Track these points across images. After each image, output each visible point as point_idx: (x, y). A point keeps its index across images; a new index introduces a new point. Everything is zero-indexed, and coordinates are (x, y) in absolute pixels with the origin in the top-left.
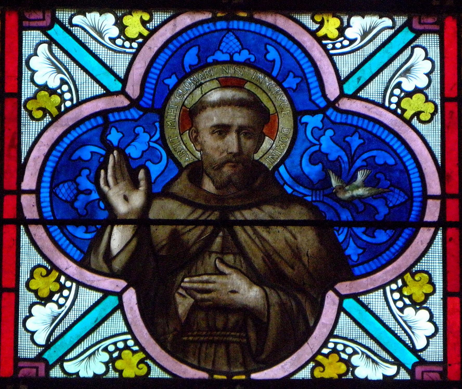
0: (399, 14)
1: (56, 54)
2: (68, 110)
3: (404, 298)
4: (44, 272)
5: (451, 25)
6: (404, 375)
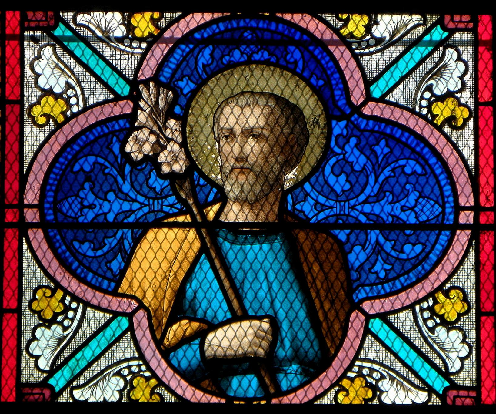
0: (66, 403)
2: (75, 115)
4: (48, 293)
5: (486, 20)
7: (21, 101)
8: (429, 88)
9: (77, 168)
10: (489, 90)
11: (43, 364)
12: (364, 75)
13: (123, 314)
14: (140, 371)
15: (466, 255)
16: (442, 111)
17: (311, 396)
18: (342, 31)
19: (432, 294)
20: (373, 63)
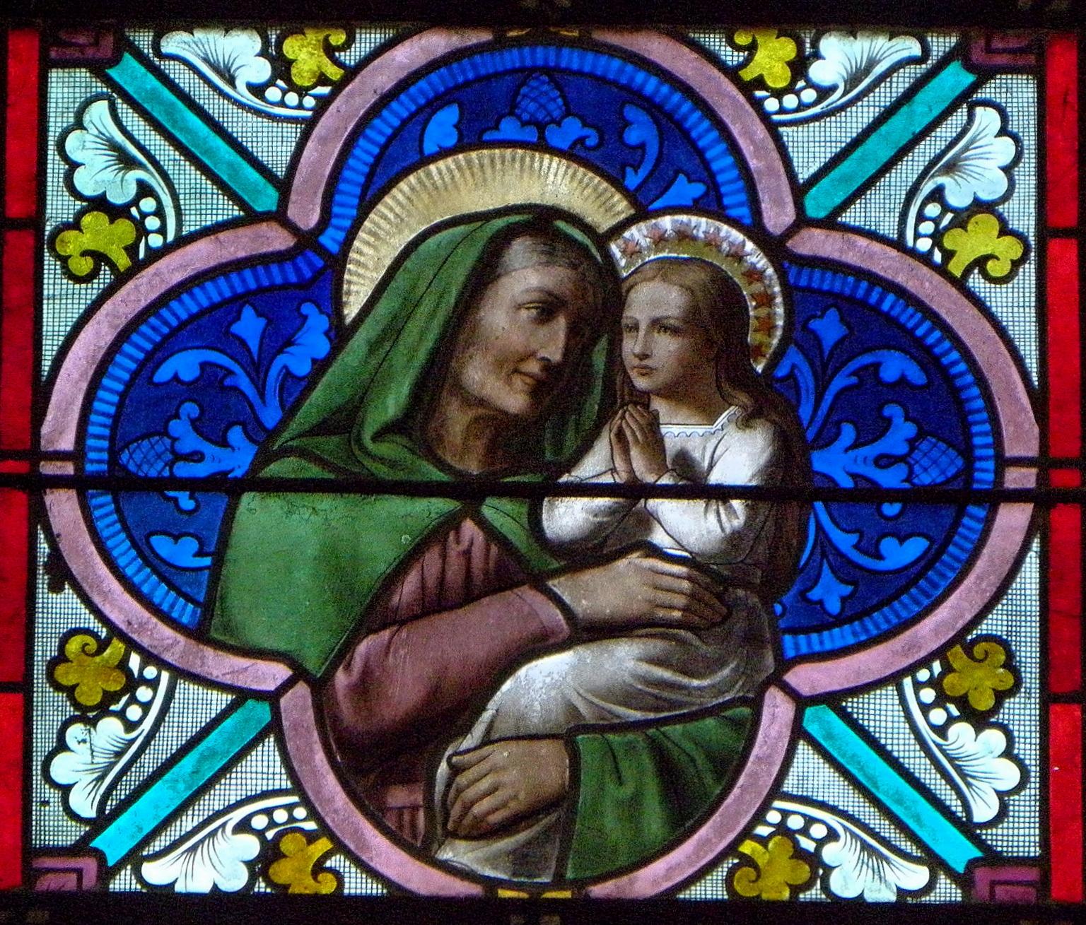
1: (129, 128)
4: (93, 645)
6: (947, 891)
11: (987, 119)
14: (292, 819)
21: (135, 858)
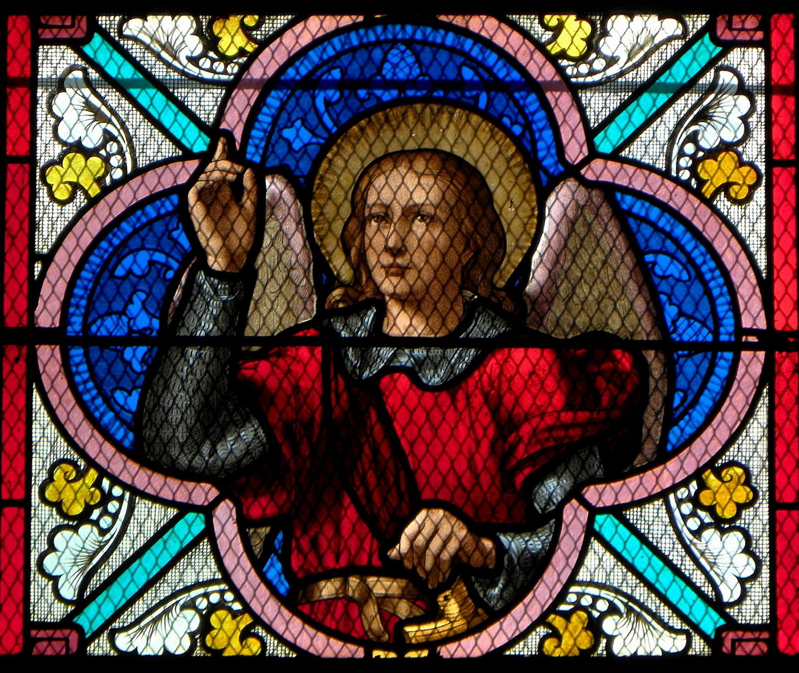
0: (105, 658)
2: (116, 184)
3: (699, 512)
5: (783, 24)
6: (699, 646)
7: (31, 158)
8: (693, 138)
9: (120, 272)
10: (792, 298)
12: (585, 120)
13: (197, 509)
15: (750, 414)
16: (715, 172)
17: (501, 641)
18: (549, 47)
19: (697, 475)
20: (598, 104)
21: (109, 629)
